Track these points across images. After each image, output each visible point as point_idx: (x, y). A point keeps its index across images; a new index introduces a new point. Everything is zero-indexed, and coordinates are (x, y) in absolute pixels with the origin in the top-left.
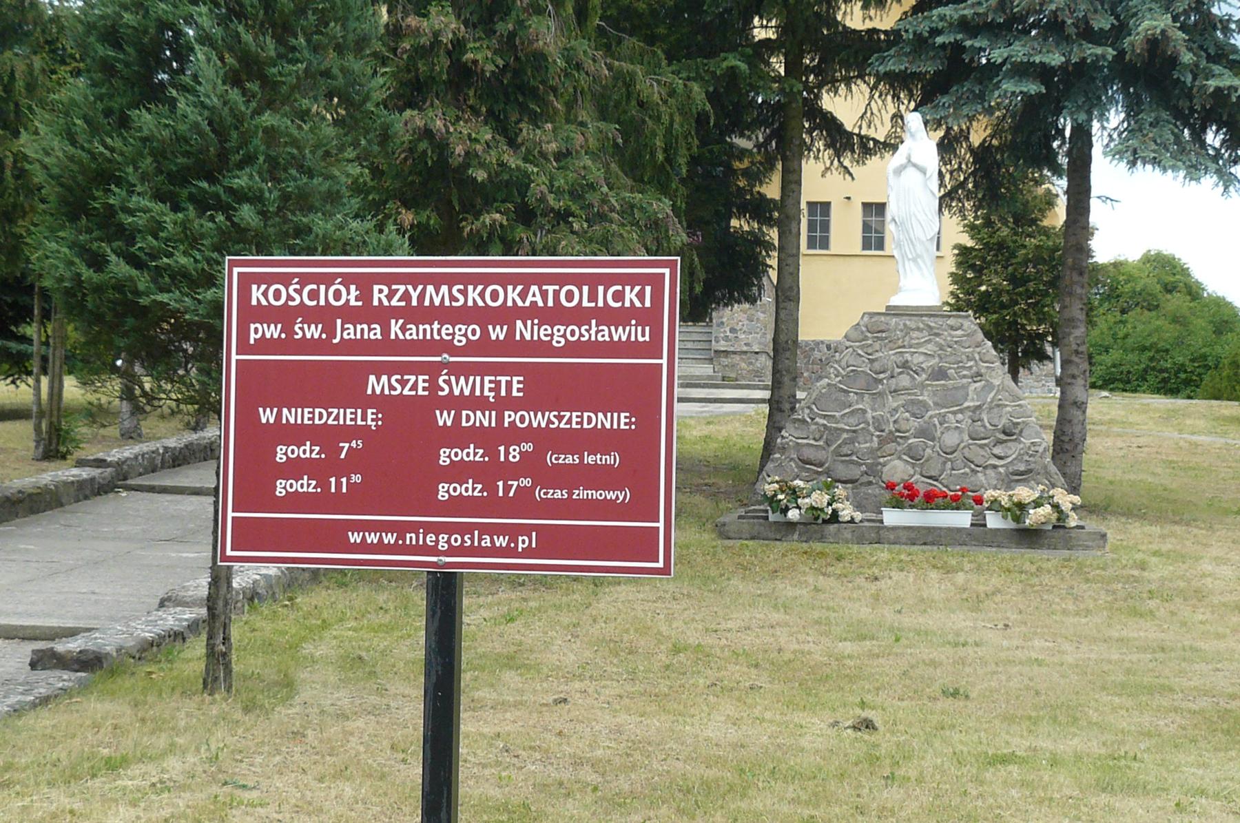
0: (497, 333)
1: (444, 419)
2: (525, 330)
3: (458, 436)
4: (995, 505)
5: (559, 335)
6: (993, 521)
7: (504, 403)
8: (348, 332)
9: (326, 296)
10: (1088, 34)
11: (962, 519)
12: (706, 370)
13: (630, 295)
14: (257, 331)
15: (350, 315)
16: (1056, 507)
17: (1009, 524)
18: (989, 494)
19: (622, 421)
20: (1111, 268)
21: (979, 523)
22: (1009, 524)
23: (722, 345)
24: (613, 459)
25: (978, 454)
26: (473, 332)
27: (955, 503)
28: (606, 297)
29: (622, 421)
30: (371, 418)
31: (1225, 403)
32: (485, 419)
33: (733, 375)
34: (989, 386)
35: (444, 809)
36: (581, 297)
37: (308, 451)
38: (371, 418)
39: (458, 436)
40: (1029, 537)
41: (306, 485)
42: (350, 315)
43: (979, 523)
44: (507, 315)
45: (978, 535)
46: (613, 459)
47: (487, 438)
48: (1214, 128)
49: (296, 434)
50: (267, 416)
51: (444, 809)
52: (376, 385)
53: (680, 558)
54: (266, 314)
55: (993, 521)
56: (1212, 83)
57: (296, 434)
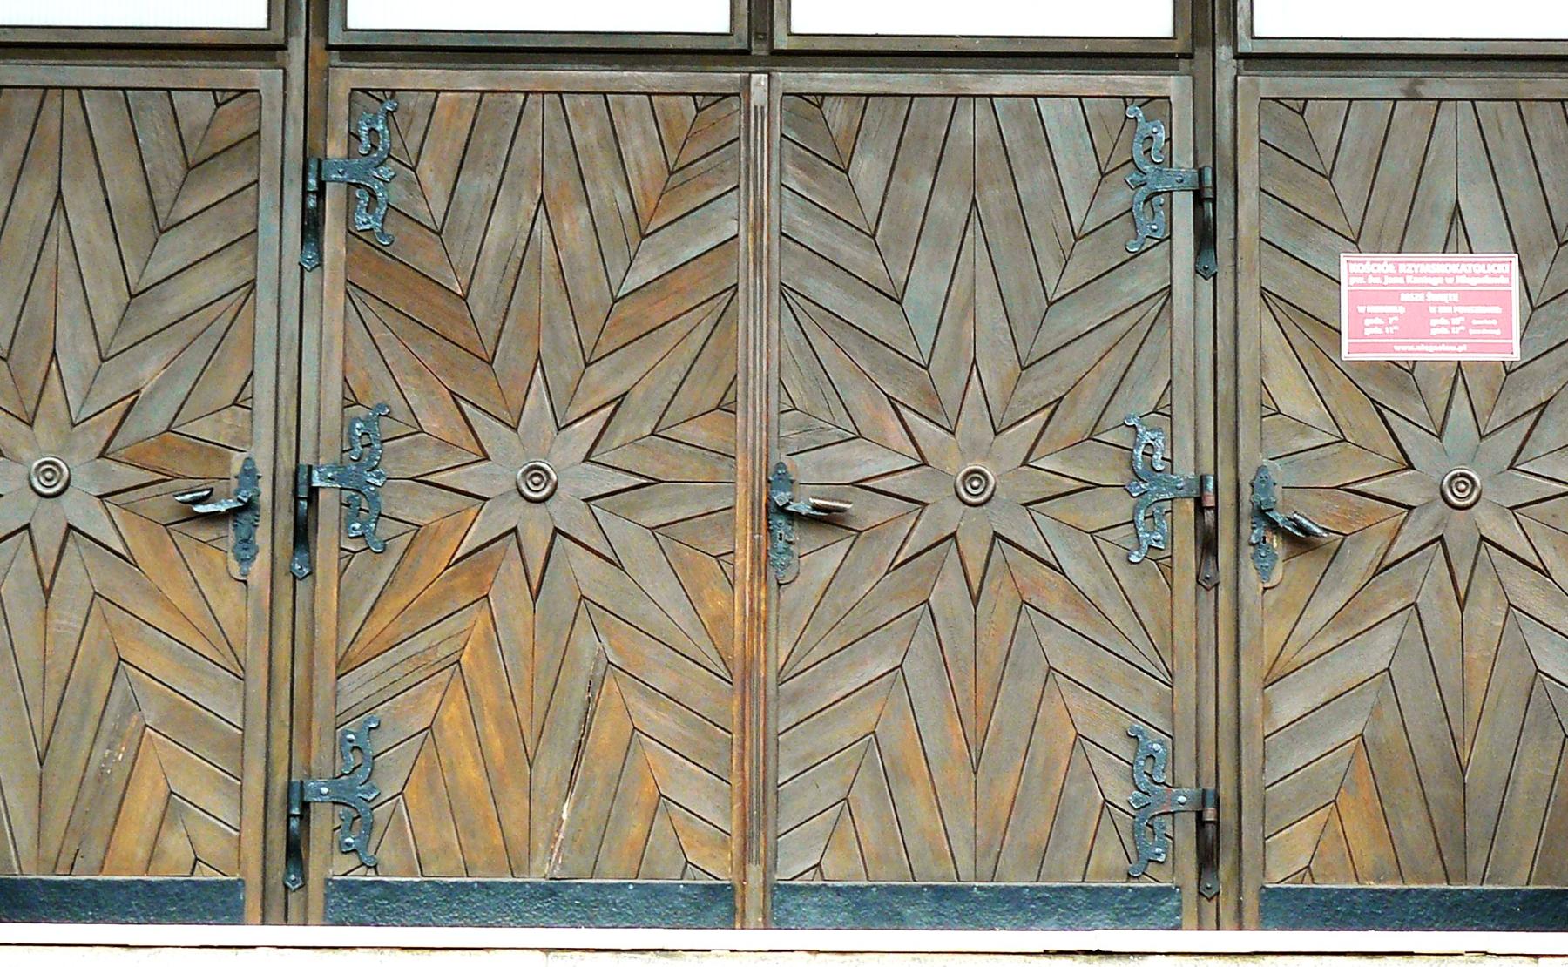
0: (1450, 280)
1: (1433, 309)
2: (1460, 280)
3: (1438, 316)
5: (1474, 281)
7: (1452, 304)
8: (1388, 280)
9: (1381, 268)
13: (1500, 267)
14: (1353, 280)
15: (1391, 275)
19: (1497, 310)
20: (1480, 213)
24: (1494, 322)
26: (1440, 280)
28: (1491, 268)
29: (1497, 310)
30: (1402, 310)
31: (1367, 257)
32: (1448, 310)
36: (1482, 268)
37: (1378, 321)
38: (1402, 310)
39: (1438, 316)
41: (1378, 331)
42: (1391, 275)
44: (1454, 275)
46: (1494, 322)
47: (1449, 316)
49: (1373, 315)
50: (1361, 309)
52: (1404, 297)
53: (85, 429)
54: (1355, 275)
57: (1373, 315)
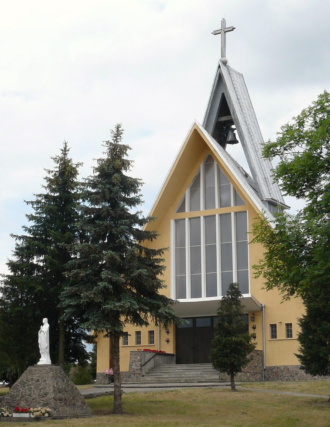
33: (225, 378)
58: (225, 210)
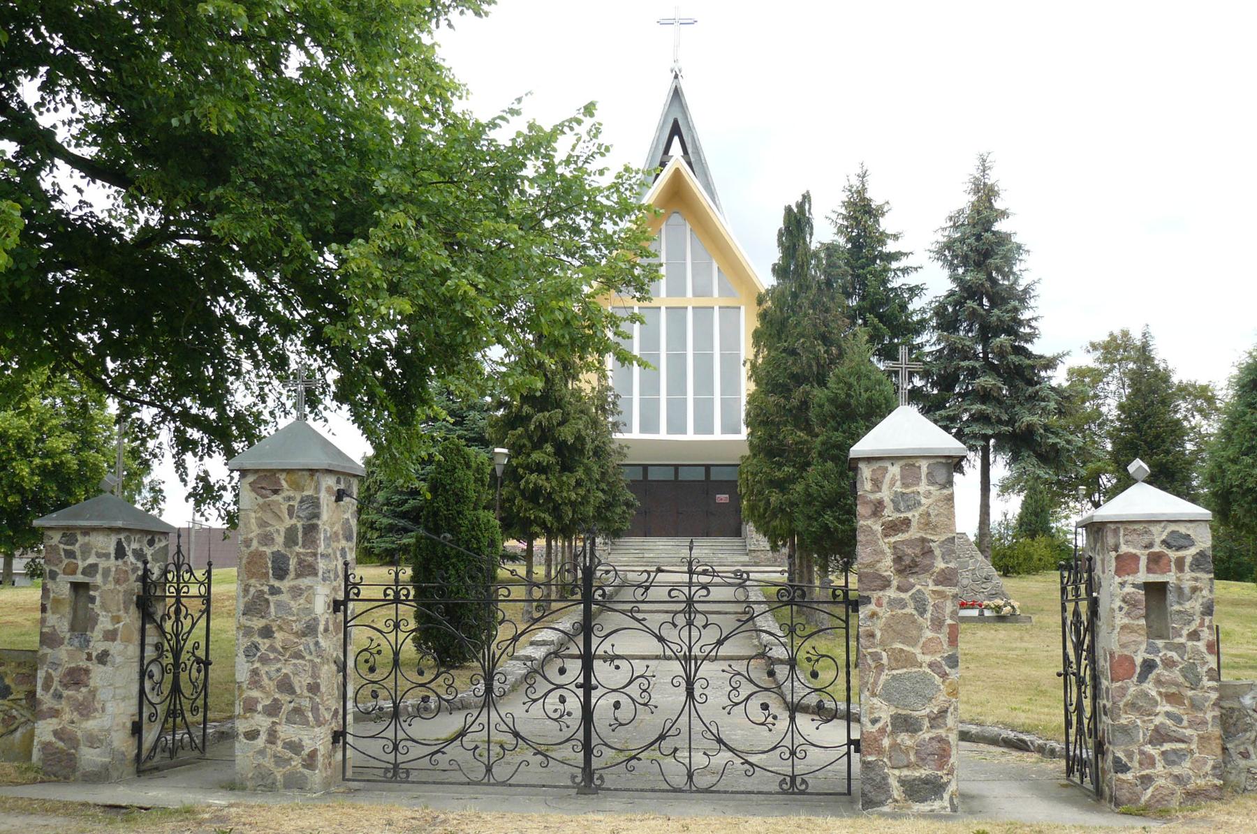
4: (987, 607)
6: (987, 613)
10: (1000, 421)
11: (975, 613)
12: (746, 558)
16: (1013, 607)
17: (994, 614)
18: (986, 603)
21: (981, 614)
22: (994, 614)
23: (753, 548)
25: (976, 588)
27: (972, 607)
34: (977, 561)
35: (1069, 622)
40: (1001, 619)
43: (981, 614)
45: (981, 619)
48: (617, 436)
51: (1069, 622)
55: (987, 613)
56: (1051, 441)
58: (703, 302)
